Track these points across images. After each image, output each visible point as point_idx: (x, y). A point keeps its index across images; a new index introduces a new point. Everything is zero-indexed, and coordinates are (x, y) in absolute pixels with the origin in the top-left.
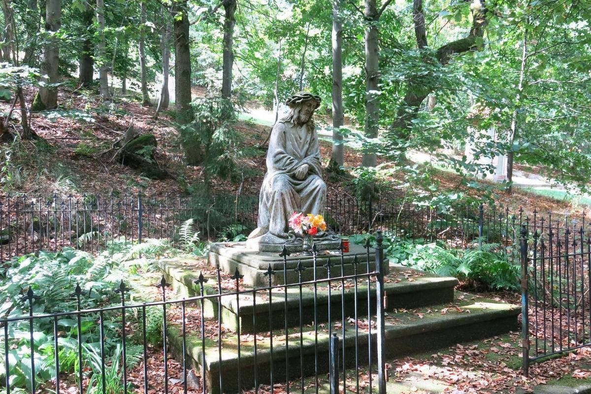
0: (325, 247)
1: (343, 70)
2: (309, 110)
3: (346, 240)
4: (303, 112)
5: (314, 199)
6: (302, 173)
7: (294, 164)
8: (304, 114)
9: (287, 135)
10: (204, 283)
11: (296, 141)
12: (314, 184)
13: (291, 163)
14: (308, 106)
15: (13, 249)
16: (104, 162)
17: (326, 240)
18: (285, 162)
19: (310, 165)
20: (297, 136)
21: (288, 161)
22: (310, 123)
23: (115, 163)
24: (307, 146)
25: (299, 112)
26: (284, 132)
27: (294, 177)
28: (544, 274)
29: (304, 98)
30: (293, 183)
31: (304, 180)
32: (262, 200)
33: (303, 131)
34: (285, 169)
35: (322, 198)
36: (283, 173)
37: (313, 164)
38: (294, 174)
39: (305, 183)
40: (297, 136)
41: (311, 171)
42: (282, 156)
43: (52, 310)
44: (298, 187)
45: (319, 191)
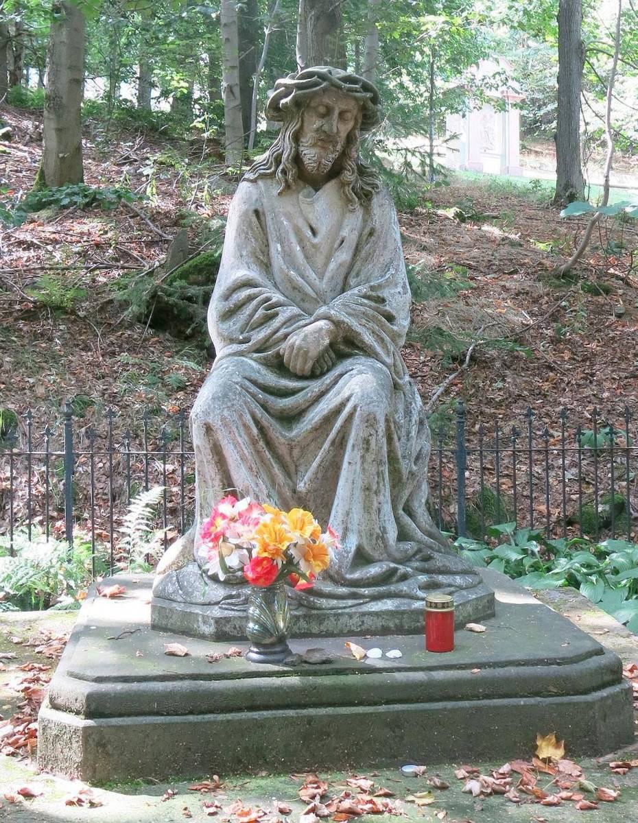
0: (379, 623)
2: (326, 128)
3: (444, 605)
4: (307, 140)
5: (340, 444)
6: (303, 353)
7: (276, 323)
8: (314, 145)
11: (301, 241)
12: (339, 393)
13: (269, 318)
14: (323, 116)
16: (99, 324)
17: (390, 596)
18: (251, 316)
19: (337, 323)
20: (301, 223)
21: (261, 312)
23: (131, 326)
24: (344, 256)
25: (297, 138)
26: (256, 212)
27: (279, 366)
29: (299, 87)
30: (266, 389)
33: (323, 207)
34: (246, 341)
35: (367, 442)
38: (279, 356)
40: (301, 223)
41: (344, 346)
43: (298, 648)
45: (355, 408)
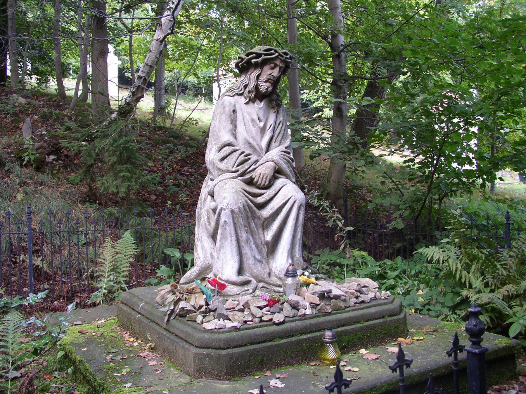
1: (153, 105)
9: (239, 115)
10: (343, 387)
15: (134, 194)
22: (275, 97)
27: (250, 182)
28: (166, 330)
29: (265, 55)
31: (267, 187)
32: (199, 221)
34: (237, 171)
36: (233, 178)
37: (281, 162)
38: (252, 179)
39: (268, 194)
42: (230, 149)
44: (260, 200)
